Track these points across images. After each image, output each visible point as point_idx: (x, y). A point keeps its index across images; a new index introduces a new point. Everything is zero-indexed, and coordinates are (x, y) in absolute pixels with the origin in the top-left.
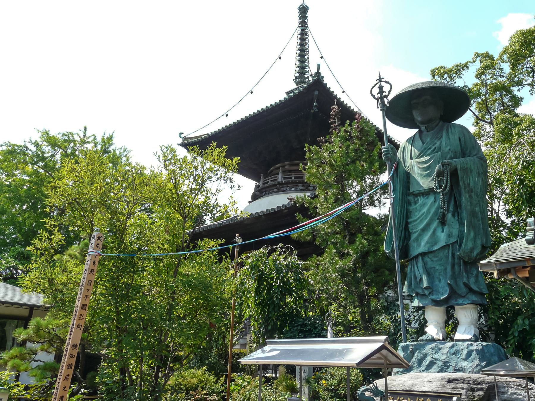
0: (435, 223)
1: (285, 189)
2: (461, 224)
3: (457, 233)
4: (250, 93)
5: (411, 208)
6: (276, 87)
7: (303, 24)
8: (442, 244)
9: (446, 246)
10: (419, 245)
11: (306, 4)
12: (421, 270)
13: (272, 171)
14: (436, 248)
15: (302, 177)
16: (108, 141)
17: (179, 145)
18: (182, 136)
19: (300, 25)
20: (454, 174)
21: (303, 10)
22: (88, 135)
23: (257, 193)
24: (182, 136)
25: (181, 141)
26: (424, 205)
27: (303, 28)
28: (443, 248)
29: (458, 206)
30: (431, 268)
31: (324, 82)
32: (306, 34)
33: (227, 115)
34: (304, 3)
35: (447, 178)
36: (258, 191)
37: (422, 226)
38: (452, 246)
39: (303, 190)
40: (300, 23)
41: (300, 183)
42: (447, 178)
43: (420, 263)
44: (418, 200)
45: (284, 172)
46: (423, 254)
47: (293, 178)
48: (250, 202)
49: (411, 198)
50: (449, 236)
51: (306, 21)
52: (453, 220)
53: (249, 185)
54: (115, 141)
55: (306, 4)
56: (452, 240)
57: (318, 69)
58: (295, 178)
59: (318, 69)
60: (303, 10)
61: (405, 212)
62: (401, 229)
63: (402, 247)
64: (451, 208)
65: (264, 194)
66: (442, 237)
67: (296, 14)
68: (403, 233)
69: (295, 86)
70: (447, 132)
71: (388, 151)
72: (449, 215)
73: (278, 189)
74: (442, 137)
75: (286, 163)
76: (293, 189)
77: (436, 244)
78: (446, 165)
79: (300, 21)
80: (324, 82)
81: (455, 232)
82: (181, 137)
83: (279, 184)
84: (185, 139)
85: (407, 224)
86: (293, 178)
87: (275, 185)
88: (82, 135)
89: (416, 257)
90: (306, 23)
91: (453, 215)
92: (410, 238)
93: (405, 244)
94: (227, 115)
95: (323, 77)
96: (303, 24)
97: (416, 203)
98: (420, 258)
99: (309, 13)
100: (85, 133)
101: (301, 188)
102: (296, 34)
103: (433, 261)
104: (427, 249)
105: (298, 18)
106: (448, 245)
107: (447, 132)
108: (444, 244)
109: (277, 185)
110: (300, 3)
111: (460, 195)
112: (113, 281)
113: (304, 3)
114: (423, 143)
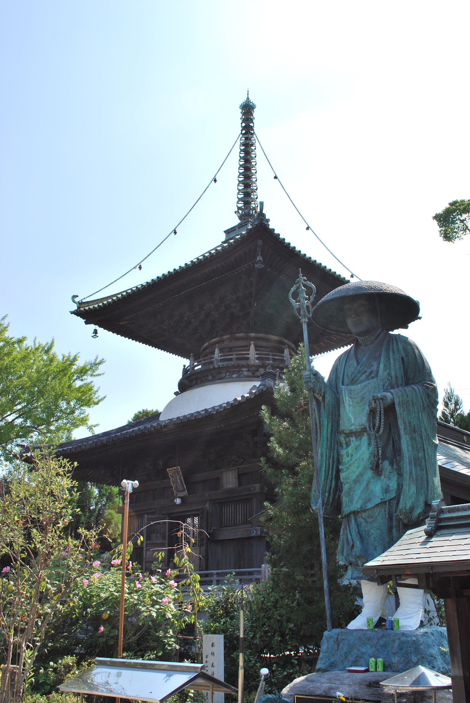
0: (369, 474)
2: (400, 475)
3: (395, 487)
4: (173, 234)
6: (205, 231)
9: (383, 503)
10: (351, 501)
11: (252, 99)
12: (354, 534)
13: (206, 348)
14: (369, 506)
17: (72, 313)
18: (77, 300)
19: (244, 132)
20: (390, 409)
21: (248, 109)
23: (186, 382)
24: (77, 300)
25: (74, 307)
26: (357, 448)
27: (247, 136)
29: (397, 451)
31: (271, 227)
32: (252, 145)
33: (140, 268)
34: (248, 98)
35: (380, 417)
38: (389, 503)
39: (249, 377)
40: (243, 128)
41: (243, 366)
42: (380, 417)
44: (350, 441)
45: (221, 351)
46: (355, 513)
48: (176, 394)
49: (342, 438)
50: (386, 490)
51: (251, 124)
53: (174, 365)
55: (253, 100)
60: (248, 109)
61: (336, 455)
62: (330, 477)
63: (333, 501)
65: (194, 383)
67: (238, 114)
68: (333, 482)
69: (240, 221)
70: (388, 350)
71: (310, 378)
73: (214, 377)
74: (380, 355)
75: (225, 337)
76: (234, 376)
77: (369, 500)
78: (378, 399)
79: (244, 125)
80: (271, 227)
81: (393, 485)
82: (74, 302)
84: (80, 304)
85: (338, 471)
89: (348, 516)
90: (252, 128)
91: (391, 464)
92: (341, 491)
93: (337, 497)
94: (140, 268)
95: (268, 220)
97: (348, 445)
98: (353, 517)
99: (256, 114)
101: (246, 373)
102: (238, 143)
103: (367, 522)
104: (359, 507)
105: (241, 121)
106: (385, 502)
107: (388, 350)
108: (379, 501)
109: (211, 370)
110: (243, 100)
111: (400, 438)
113: (248, 98)
114: (358, 363)
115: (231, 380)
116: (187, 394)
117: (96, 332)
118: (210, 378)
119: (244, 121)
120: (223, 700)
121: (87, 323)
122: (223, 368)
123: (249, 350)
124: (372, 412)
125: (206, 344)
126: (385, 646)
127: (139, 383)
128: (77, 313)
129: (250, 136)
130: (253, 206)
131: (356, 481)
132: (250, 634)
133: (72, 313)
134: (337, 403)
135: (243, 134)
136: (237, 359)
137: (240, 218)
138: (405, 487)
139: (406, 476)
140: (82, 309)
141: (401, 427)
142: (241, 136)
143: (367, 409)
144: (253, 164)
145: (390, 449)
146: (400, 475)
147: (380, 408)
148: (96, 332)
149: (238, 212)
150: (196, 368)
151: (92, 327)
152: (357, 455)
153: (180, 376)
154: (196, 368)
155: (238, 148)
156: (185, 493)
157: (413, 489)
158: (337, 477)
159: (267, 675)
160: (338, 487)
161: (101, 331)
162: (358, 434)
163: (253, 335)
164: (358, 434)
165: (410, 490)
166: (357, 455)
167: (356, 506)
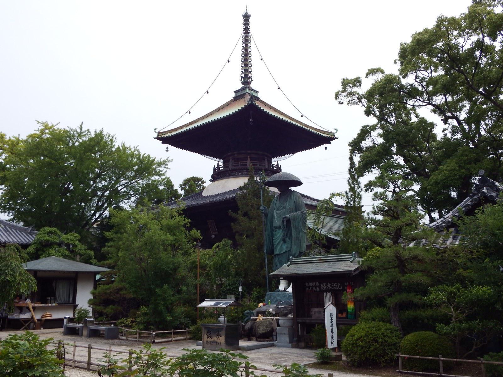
0: (282, 242)
1: (234, 174)
5: (274, 233)
7: (246, 31)
8: (284, 251)
11: (249, 11)
14: (282, 253)
15: (246, 165)
19: (244, 32)
21: (246, 17)
22: (83, 130)
24: (157, 131)
25: (156, 135)
26: (278, 233)
27: (246, 35)
28: (284, 253)
29: (291, 235)
30: (150, 347)
33: (190, 113)
36: (216, 174)
37: (277, 243)
41: (244, 169)
43: (277, 259)
47: (240, 166)
50: (287, 248)
51: (248, 27)
52: (289, 240)
54: (103, 131)
56: (288, 249)
57: (246, 79)
58: (241, 165)
59: (246, 79)
60: (246, 17)
64: (288, 235)
67: (241, 21)
72: (288, 239)
75: (235, 153)
76: (240, 174)
79: (244, 27)
81: (289, 246)
82: (155, 132)
83: (230, 170)
84: (159, 133)
86: (240, 166)
87: (227, 171)
88: (79, 131)
89: (275, 255)
91: (289, 239)
94: (190, 113)
96: (246, 31)
97: (276, 231)
99: (251, 20)
100: (81, 129)
107: (290, 198)
110: (243, 12)
115: (239, 176)
116: (216, 183)
117: (167, 148)
120: (21, 127)
121: (163, 143)
122: (234, 170)
123: (247, 161)
124: (283, 221)
126: (284, 297)
127: (189, 167)
128: (157, 138)
129: (248, 35)
131: (278, 244)
132: (477, 99)
135: (244, 33)
136: (241, 165)
137: (243, 83)
138: (293, 247)
139: (293, 243)
140: (160, 137)
141: (292, 227)
142: (243, 34)
143: (282, 221)
145: (289, 234)
146: (291, 243)
147: (285, 220)
148: (167, 148)
149: (241, 80)
150: (220, 169)
151: (166, 145)
152: (279, 234)
153: (212, 173)
154: (220, 169)
156: (217, 233)
157: (295, 247)
158: (272, 242)
160: (273, 245)
161: (170, 147)
162: (279, 228)
163: (249, 152)
164: (279, 228)
165: (295, 247)
166: (279, 234)
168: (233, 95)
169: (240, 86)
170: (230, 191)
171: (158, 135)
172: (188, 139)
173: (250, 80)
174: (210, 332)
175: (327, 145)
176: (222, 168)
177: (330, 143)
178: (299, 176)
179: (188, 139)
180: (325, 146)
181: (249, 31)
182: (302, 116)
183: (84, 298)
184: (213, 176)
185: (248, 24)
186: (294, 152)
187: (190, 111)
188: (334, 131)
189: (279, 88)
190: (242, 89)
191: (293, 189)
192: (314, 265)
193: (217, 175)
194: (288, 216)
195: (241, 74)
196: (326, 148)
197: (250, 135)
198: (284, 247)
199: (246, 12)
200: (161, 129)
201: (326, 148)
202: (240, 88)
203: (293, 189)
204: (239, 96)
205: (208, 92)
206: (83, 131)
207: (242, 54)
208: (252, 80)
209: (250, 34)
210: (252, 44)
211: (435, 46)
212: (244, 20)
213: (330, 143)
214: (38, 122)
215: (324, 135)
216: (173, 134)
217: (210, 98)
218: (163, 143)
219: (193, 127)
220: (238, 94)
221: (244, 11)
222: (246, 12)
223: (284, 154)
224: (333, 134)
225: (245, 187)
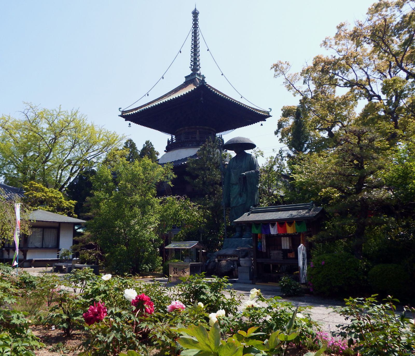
4: (162, 78)
7: (195, 26)
11: (197, 9)
14: (238, 205)
15: (196, 138)
16: (369, 9)
17: (119, 116)
18: (121, 110)
21: (195, 14)
24: (121, 110)
27: (195, 29)
34: (195, 8)
46: (234, 207)
47: (190, 138)
51: (197, 23)
57: (195, 66)
59: (195, 66)
60: (195, 14)
66: (240, 200)
67: (191, 17)
76: (190, 145)
82: (120, 111)
84: (123, 112)
86: (190, 138)
94: (148, 95)
96: (195, 26)
99: (199, 17)
112: (298, 108)
113: (195, 8)
114: (236, 163)
116: (170, 153)
117: (130, 124)
118: (180, 146)
119: (194, 20)
121: (126, 120)
124: (240, 179)
125: (177, 130)
128: (122, 116)
130: (198, 64)
133: (119, 116)
134: (230, 175)
135: (194, 28)
137: (192, 70)
140: (124, 115)
142: (193, 28)
144: (198, 39)
148: (130, 124)
149: (191, 67)
151: (129, 122)
153: (167, 145)
154: (174, 141)
155: (190, 36)
159: (223, 141)
161: (132, 123)
162: (236, 184)
163: (198, 127)
167: (234, 205)
168: (184, 80)
169: (189, 72)
170: (182, 159)
171: (122, 114)
172: (145, 117)
173: (199, 67)
174: (176, 269)
175: (263, 122)
176: (175, 141)
177: (265, 120)
178: (253, 141)
179: (145, 117)
180: (261, 122)
181: (197, 26)
182: (241, 97)
183: (66, 243)
184: (167, 148)
185: (197, 20)
186: (235, 128)
187: (149, 93)
188: (269, 110)
189: (222, 75)
190: (192, 75)
191: (248, 152)
192: (261, 214)
193: (170, 147)
194: (244, 174)
195: (191, 63)
196: (262, 125)
197: (197, 113)
198: (240, 200)
199: (195, 10)
200: (124, 108)
201: (262, 125)
202: (190, 74)
203: (248, 152)
204: (189, 80)
205: (163, 78)
206: (61, 111)
207: (192, 45)
208: (200, 68)
209: (198, 28)
210: (200, 37)
211: (202, 102)
212: (194, 17)
213: (265, 120)
214: (24, 103)
215: (261, 113)
216: (130, 113)
217: (164, 82)
218: (126, 120)
219: (150, 107)
220: (189, 79)
221: (193, 9)
222: (195, 10)
223: (226, 130)
224: (268, 113)
225: (195, 155)
